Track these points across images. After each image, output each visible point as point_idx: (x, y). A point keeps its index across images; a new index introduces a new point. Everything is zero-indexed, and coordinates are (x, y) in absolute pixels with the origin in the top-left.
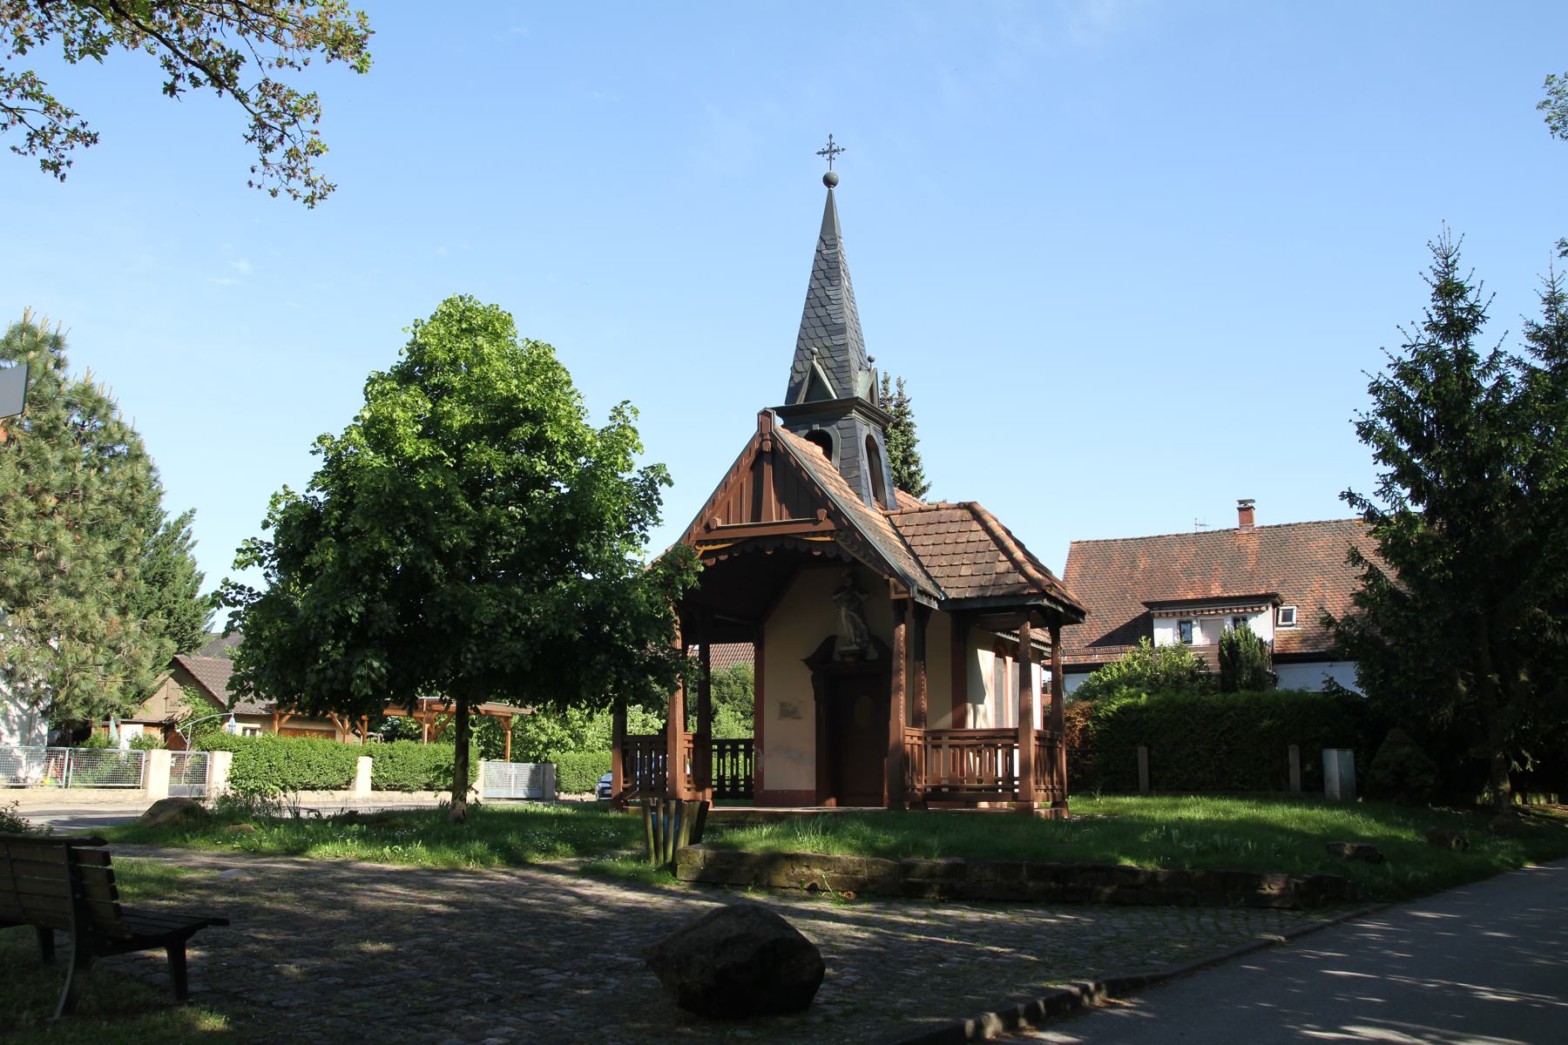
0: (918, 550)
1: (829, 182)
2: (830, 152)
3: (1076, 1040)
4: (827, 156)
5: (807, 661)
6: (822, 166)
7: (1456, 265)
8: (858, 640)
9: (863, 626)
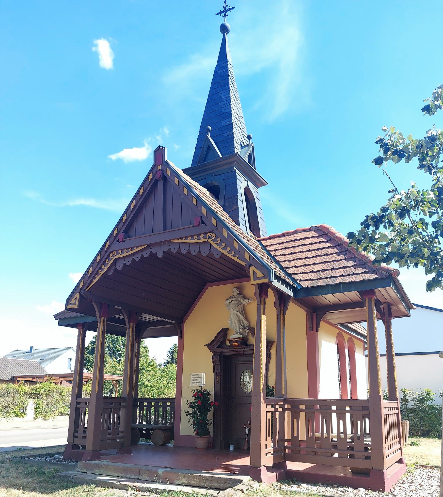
0: (279, 259)
1: (224, 29)
2: (225, 11)
3: (315, 464)
4: (223, 14)
5: (208, 346)
6: (220, 20)
7: (426, 464)
8: (241, 330)
9: (245, 322)
